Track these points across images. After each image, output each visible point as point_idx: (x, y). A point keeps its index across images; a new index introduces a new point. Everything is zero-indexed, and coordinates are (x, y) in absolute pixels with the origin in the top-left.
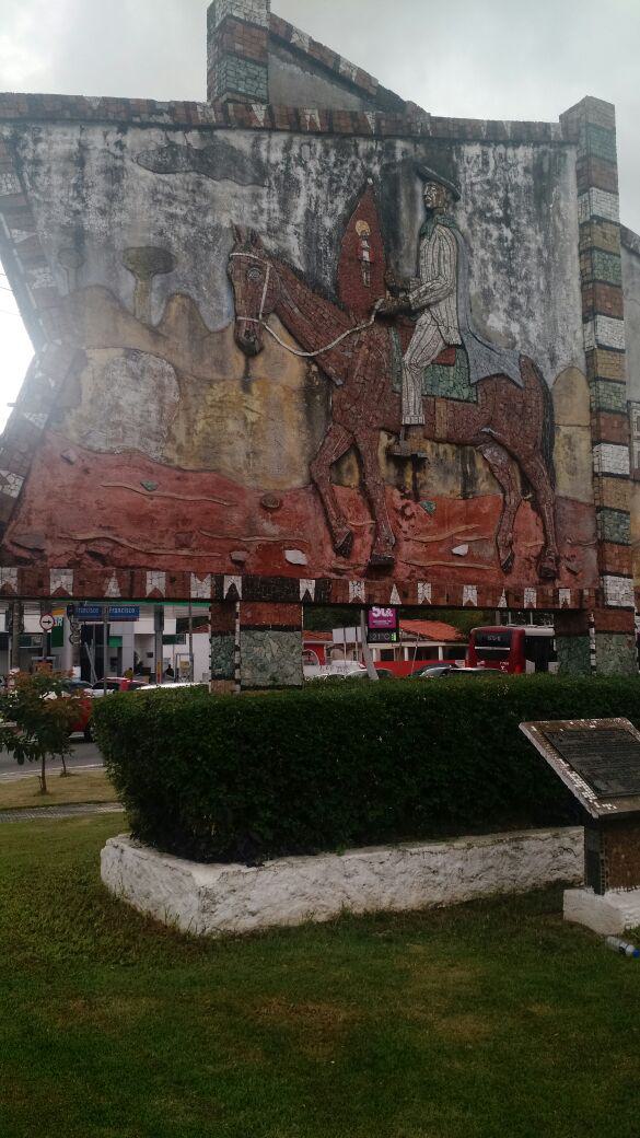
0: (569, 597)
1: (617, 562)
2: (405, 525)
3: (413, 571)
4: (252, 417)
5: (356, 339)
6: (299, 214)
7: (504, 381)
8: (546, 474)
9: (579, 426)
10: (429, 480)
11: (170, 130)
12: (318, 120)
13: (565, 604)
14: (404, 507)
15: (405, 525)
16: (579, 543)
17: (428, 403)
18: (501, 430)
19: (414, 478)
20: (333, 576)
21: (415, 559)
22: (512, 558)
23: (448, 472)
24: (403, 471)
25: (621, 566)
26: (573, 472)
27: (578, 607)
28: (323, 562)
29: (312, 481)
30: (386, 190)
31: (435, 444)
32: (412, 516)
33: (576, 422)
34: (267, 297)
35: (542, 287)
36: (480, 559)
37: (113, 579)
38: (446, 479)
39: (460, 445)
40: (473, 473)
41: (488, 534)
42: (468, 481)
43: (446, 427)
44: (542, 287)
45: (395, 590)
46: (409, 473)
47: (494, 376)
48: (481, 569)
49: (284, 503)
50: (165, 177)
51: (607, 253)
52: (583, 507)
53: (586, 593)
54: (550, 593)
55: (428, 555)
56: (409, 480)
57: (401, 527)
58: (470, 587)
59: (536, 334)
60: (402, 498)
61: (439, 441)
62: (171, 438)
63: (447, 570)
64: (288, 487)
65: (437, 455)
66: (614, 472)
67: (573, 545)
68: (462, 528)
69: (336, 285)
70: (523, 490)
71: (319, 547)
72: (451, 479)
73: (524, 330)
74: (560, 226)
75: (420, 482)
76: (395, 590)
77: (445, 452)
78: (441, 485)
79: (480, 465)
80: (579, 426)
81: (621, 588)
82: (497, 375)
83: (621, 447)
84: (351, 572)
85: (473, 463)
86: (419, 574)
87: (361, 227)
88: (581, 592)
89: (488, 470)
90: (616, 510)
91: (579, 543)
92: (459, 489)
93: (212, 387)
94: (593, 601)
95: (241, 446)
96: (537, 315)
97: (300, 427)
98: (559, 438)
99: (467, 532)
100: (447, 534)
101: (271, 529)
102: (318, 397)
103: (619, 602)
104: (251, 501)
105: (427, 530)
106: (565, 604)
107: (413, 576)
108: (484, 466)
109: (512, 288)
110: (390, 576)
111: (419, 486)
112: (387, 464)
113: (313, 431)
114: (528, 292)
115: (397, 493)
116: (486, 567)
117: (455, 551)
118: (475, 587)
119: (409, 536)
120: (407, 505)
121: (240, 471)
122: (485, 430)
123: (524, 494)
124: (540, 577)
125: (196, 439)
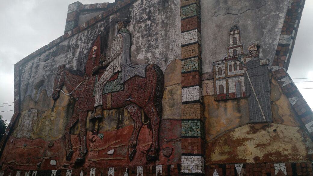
0: (161, 169)
1: (190, 148)
2: (91, 145)
3: (91, 164)
4: (52, 118)
5: (84, 84)
6: (77, 54)
7: (137, 78)
8: (154, 110)
9: (177, 84)
10: (104, 125)
11: (50, 50)
12: (85, 26)
13: (159, 173)
14: (92, 138)
15: (91, 145)
16: (171, 140)
17: (104, 97)
18: (134, 98)
19: (99, 126)
20: (64, 168)
21: (93, 158)
22: (135, 152)
23: (112, 120)
24: (95, 124)
25: (193, 149)
26: (172, 106)
27: (167, 174)
28: (62, 163)
29: (64, 136)
30: (105, 33)
31: (108, 111)
32: (95, 141)
33: (176, 83)
34: (60, 82)
35: (163, 34)
36: (120, 155)
37: (10, 174)
38: (111, 123)
39: (118, 108)
40: (122, 118)
41: (125, 143)
42: (120, 122)
43: (110, 103)
44: (163, 34)
45: (82, 172)
46: (97, 124)
47: (133, 77)
48: (119, 159)
49: (55, 144)
50: (46, 62)
51: (187, 6)
52: (176, 121)
53: (173, 166)
54: (151, 168)
55: (99, 156)
56: (96, 127)
57: (90, 146)
58: (112, 168)
59: (158, 53)
60: (92, 134)
61: (110, 109)
62: (32, 130)
63: (104, 162)
64: (58, 138)
65: (109, 115)
66: (189, 100)
67: (167, 142)
68: (113, 142)
69: (85, 69)
70: (145, 120)
71: (62, 158)
72: (113, 123)
73: (153, 54)
74: (173, 7)
75: (101, 127)
76: (82, 172)
77: (112, 113)
78: (108, 126)
79: (126, 114)
80: (177, 84)
81: (192, 162)
82: (134, 77)
83: (195, 87)
84: (69, 166)
85: (123, 114)
86: (93, 165)
87: (48, 47)
88: (169, 166)
89: (129, 115)
90: (189, 120)
91: (171, 140)
92: (115, 126)
93: (44, 113)
94: (176, 171)
95: (48, 128)
96: (160, 46)
97: (64, 118)
98: (166, 92)
99: (116, 144)
100: (108, 146)
101: (49, 153)
102: (71, 107)
103: (190, 170)
104: (46, 145)
105: (100, 145)
106: (159, 173)
107: (91, 166)
108: (128, 114)
109: (149, 41)
110: (82, 166)
111: (100, 128)
112: (90, 123)
113: (68, 118)
114: (156, 39)
115: (91, 133)
116: (122, 158)
117: (109, 153)
118: (113, 168)
119: (92, 149)
120: (94, 137)
121: (46, 136)
122: (128, 99)
123: (145, 122)
124: (147, 160)
125: (38, 129)
